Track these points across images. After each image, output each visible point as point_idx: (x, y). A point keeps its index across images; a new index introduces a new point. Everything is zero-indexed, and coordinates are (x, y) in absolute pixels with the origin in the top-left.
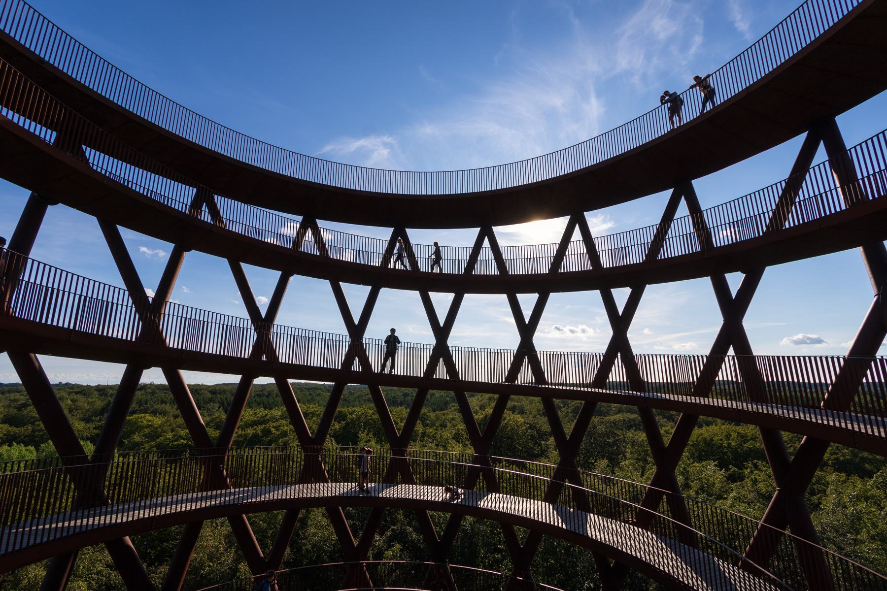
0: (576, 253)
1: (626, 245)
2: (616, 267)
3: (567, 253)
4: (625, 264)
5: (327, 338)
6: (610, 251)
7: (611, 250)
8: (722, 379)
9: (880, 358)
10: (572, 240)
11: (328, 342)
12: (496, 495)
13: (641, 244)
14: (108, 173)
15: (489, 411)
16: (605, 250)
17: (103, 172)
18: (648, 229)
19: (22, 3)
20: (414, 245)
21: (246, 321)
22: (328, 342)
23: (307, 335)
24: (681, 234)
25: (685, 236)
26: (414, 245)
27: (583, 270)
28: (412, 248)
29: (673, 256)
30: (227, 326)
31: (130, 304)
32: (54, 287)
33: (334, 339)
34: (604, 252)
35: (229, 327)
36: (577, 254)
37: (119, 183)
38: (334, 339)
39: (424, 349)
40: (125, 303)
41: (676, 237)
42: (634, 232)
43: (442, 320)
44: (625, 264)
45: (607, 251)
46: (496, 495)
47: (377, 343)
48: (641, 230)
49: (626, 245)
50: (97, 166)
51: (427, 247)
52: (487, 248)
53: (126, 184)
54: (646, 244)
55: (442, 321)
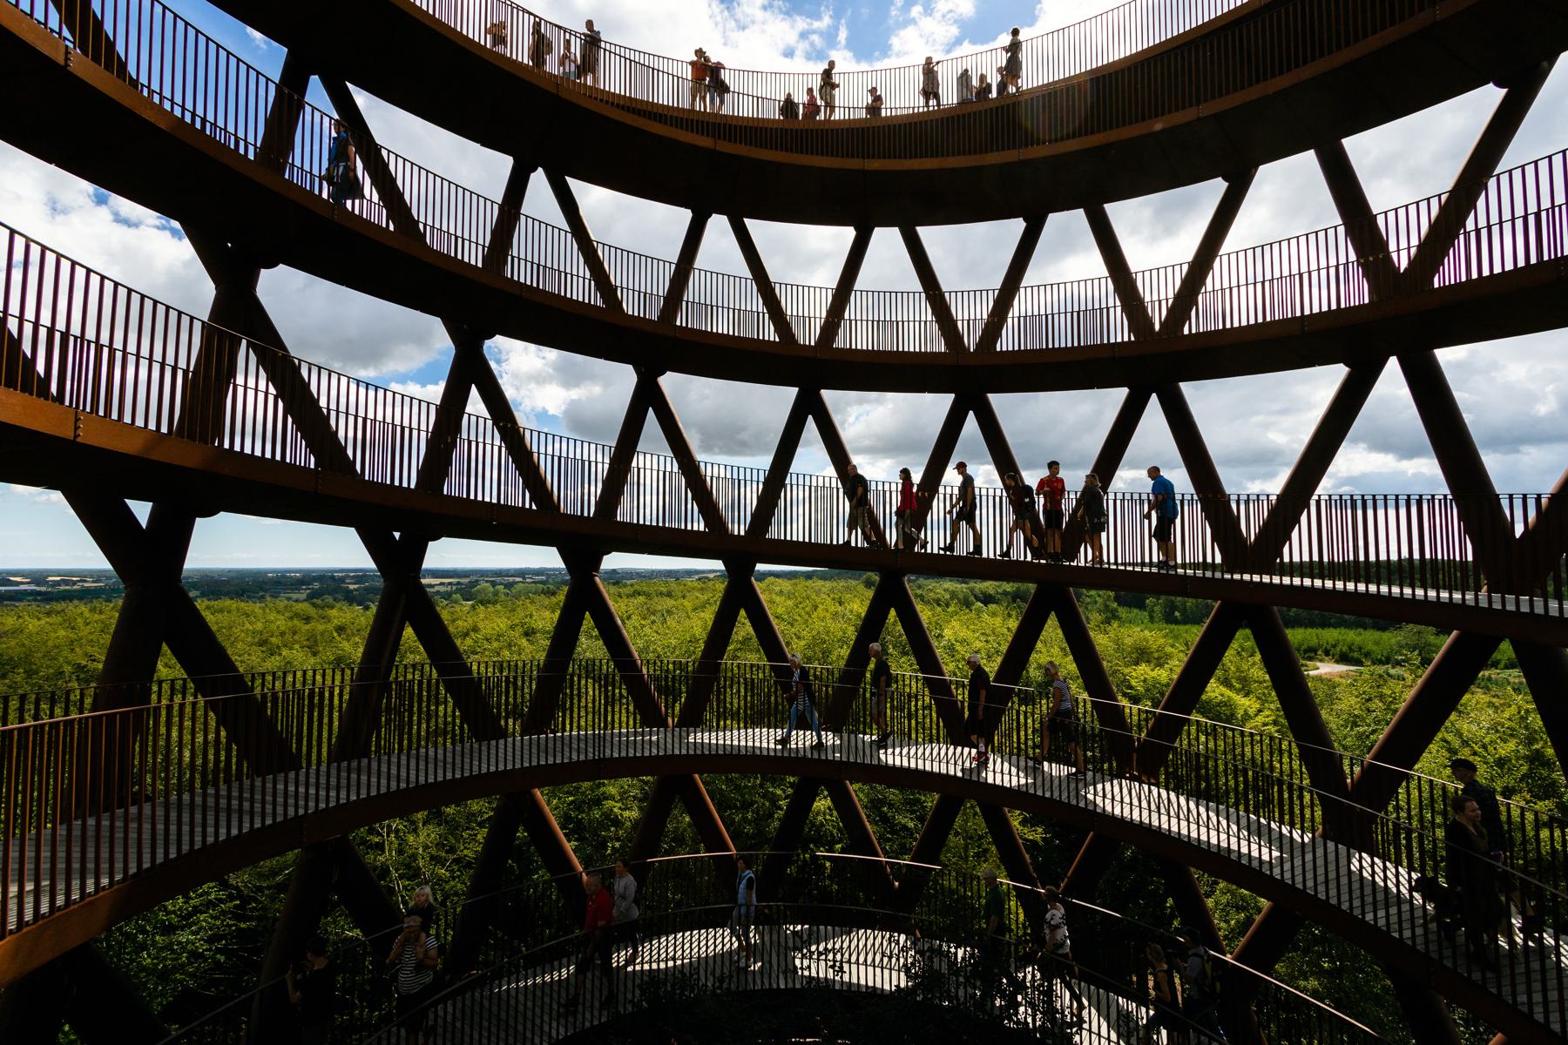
0: (1069, 309)
1: (1304, 269)
2: (1349, 309)
3: (1470, 224)
4: (1105, 342)
5: (814, 484)
6: (1075, 314)
7: (1078, 313)
8: (1385, 558)
9: (1430, 497)
10: (1224, 249)
11: (816, 491)
12: (955, 749)
13: (1072, 313)
14: (198, 121)
15: (1166, 675)
16: (1066, 313)
17: (188, 119)
18: (1155, 273)
19: (158, 9)
20: (778, 286)
21: (481, 421)
22: (816, 491)
23: (735, 476)
24: (1069, 309)
25: (1075, 314)
26: (778, 286)
27: (1268, 319)
28: (773, 290)
29: (1057, 346)
30: (560, 458)
31: (262, 386)
32: (115, 347)
33: (827, 485)
34: (1063, 316)
35: (563, 459)
36: (1072, 313)
37: (225, 147)
38: (827, 485)
39: (891, 492)
40: (489, 441)
41: (1066, 313)
42: (1089, 283)
43: (811, 427)
44: (1105, 342)
45: (1069, 315)
46: (955, 749)
47: (807, 483)
48: (1162, 272)
49: (1304, 269)
50: (183, 108)
51: (795, 288)
52: (917, 295)
53: (242, 151)
54: (1341, 268)
55: (811, 425)
